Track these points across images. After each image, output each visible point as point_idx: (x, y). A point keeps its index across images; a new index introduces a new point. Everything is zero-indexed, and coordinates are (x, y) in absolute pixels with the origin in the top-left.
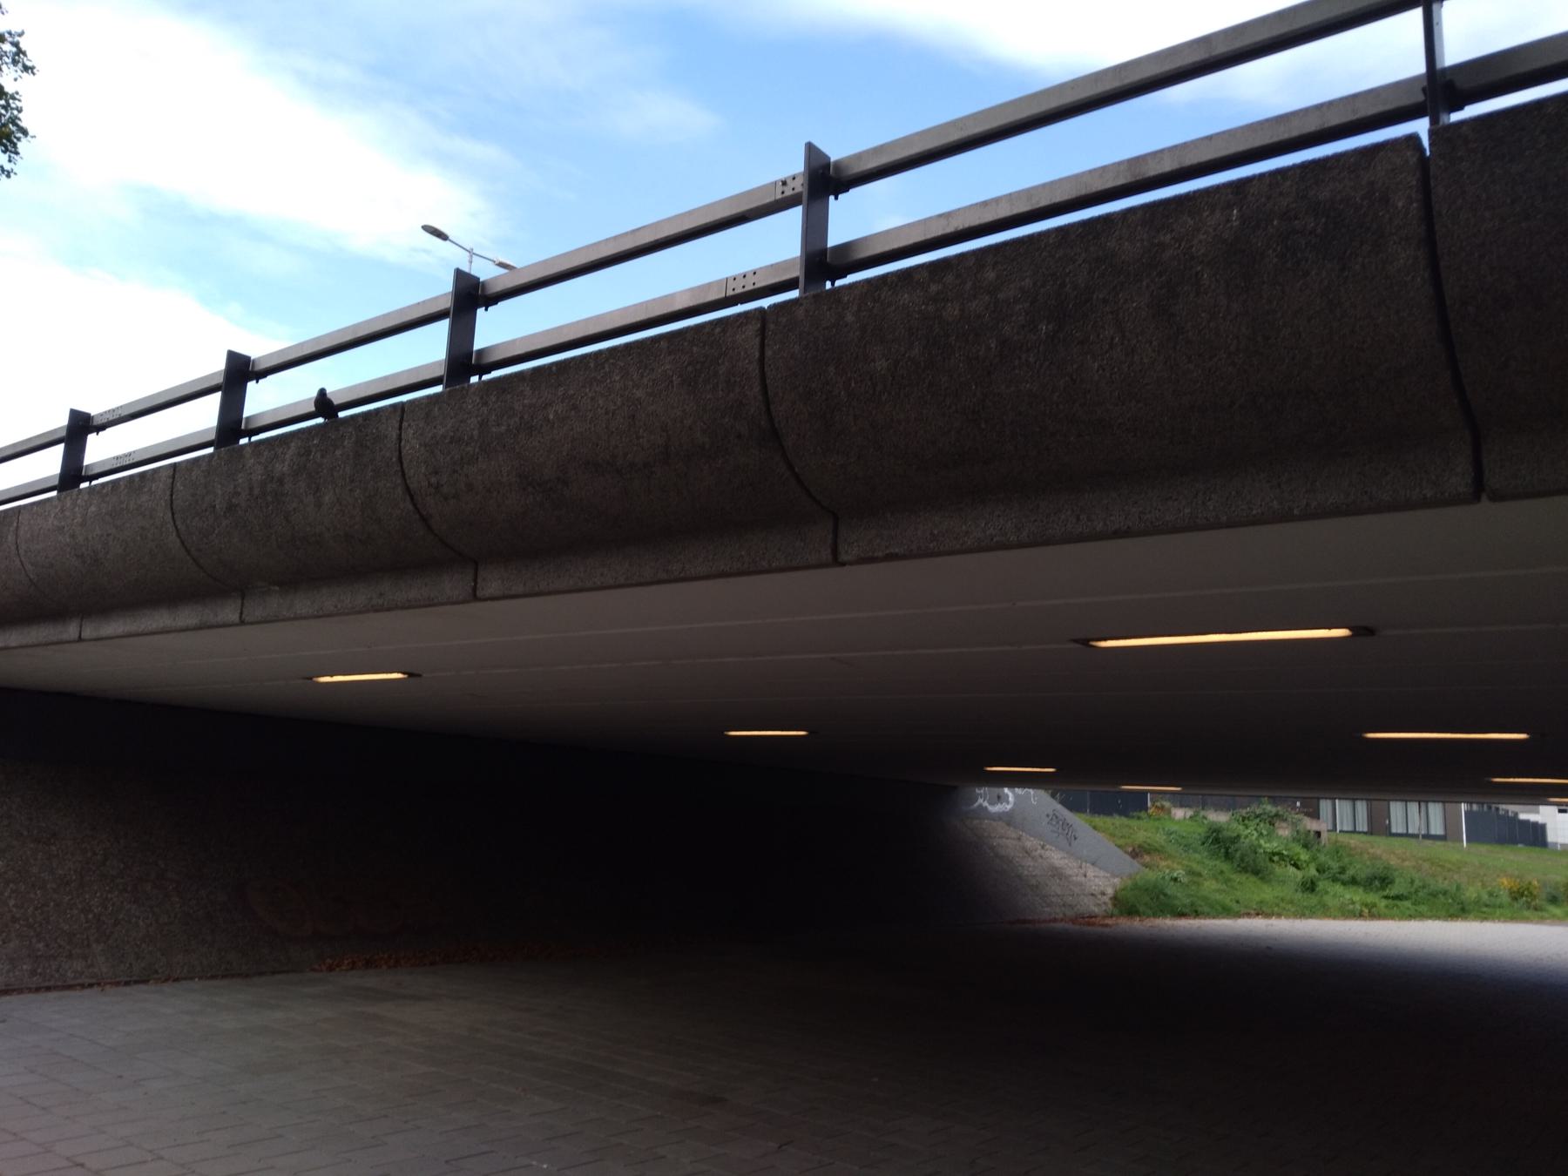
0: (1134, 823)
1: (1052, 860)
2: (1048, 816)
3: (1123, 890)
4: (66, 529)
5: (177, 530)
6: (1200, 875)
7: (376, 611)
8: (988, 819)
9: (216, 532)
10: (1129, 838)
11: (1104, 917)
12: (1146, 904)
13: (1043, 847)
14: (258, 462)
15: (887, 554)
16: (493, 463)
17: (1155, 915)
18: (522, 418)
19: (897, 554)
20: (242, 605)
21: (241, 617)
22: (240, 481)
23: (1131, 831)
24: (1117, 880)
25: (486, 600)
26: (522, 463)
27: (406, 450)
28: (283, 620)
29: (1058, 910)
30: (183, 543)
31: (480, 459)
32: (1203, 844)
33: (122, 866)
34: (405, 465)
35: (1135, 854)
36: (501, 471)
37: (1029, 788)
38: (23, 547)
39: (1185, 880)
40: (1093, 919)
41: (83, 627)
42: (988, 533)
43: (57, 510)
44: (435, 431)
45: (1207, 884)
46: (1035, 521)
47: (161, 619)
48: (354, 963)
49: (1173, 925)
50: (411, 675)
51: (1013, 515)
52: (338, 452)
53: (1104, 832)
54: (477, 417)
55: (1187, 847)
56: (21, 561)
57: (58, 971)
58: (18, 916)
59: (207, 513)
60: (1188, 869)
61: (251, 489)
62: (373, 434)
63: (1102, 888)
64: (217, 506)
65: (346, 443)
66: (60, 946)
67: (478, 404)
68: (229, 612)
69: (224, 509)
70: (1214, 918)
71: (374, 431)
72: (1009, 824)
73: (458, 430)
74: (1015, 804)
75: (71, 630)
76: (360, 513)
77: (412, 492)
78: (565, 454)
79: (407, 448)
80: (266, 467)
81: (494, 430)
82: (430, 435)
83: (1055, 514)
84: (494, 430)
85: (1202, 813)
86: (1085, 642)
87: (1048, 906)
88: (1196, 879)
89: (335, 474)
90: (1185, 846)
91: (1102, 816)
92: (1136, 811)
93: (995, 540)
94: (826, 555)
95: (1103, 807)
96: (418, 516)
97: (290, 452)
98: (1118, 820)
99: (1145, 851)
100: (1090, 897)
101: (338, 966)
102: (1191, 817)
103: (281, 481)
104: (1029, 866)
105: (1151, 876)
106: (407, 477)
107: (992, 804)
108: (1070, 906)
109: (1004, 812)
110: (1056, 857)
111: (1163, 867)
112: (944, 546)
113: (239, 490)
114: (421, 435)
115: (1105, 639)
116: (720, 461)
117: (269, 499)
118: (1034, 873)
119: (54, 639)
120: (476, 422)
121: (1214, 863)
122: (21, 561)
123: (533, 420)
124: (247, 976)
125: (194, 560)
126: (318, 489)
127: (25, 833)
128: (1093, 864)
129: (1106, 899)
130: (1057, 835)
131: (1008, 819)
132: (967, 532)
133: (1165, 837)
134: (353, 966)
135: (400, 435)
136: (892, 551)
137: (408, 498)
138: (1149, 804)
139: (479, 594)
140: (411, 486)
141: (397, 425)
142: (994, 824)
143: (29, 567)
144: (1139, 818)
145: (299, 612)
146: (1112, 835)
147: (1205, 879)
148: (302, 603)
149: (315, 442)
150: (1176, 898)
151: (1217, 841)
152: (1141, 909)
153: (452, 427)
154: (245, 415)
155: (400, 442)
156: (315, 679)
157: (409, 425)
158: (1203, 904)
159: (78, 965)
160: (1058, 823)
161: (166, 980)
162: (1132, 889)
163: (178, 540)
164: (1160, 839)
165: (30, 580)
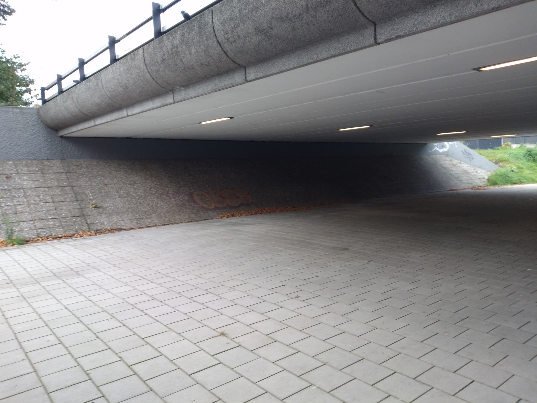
0: (496, 151)
1: (464, 168)
2: (462, 151)
3: (491, 176)
4: (115, 78)
5: (148, 71)
6: (522, 168)
7: (215, 91)
8: (439, 155)
9: (160, 70)
10: (494, 157)
11: (484, 186)
12: (500, 180)
13: (460, 163)
14: (169, 42)
15: (396, 36)
16: (245, 25)
17: (504, 184)
18: (253, 5)
19: (400, 35)
20: (173, 96)
21: (174, 100)
22: (164, 49)
23: (495, 154)
24: (489, 173)
25: (250, 81)
26: (255, 23)
27: (216, 27)
28: (187, 99)
29: (466, 185)
30: (151, 76)
31: (241, 25)
32: (524, 156)
33: (156, 190)
34: (216, 33)
35: (496, 163)
36: (248, 28)
37: (455, 141)
38: (104, 86)
39: (516, 171)
40: (480, 187)
41: (128, 111)
42: (438, 19)
43: (111, 71)
44: (224, 17)
45: (525, 171)
46: (457, 10)
47: (149, 105)
48: (228, 216)
49: (511, 187)
50: (231, 118)
51: (448, 10)
52: (193, 32)
53: (484, 155)
54: (237, 8)
55: (518, 158)
56: (105, 91)
57: (144, 222)
58: (130, 207)
59: (157, 64)
60: (518, 166)
61: (168, 52)
62: (204, 22)
63: (483, 176)
64: (159, 60)
65: (195, 28)
66: (143, 215)
67: (237, 3)
68: (169, 99)
69: (161, 61)
70: (528, 183)
71: (204, 21)
72: (447, 156)
73: (232, 15)
74: (449, 148)
75: (124, 113)
76: (204, 54)
77: (220, 43)
78: (270, 16)
79: (216, 26)
80: (171, 43)
81: (244, 12)
82: (223, 19)
83: (467, 5)
84: (244, 12)
85: (524, 145)
86: (478, 69)
87: (463, 184)
88: (521, 170)
89: (194, 41)
90: (517, 158)
91: (483, 150)
92: (496, 146)
93: (440, 22)
94: (372, 41)
95: (484, 146)
96: (223, 52)
97: (178, 36)
98: (490, 151)
99: (500, 161)
100: (479, 180)
101: (224, 217)
102: (519, 147)
103: (177, 47)
104: (455, 170)
105: (503, 170)
106: (217, 37)
107: (440, 149)
108: (471, 183)
109: (445, 152)
110: (465, 166)
111: (508, 166)
112: (420, 28)
113: (165, 53)
114: (220, 19)
115: (486, 67)
116: (328, 8)
117: (174, 54)
118: (457, 173)
119: (120, 117)
120: (237, 10)
121: (529, 163)
122: (105, 91)
123: (257, 5)
124: (198, 221)
125: (156, 82)
126: (189, 48)
127: (126, 182)
128: (480, 168)
129: (485, 180)
130: (465, 158)
131: (446, 154)
132: (429, 21)
133: (508, 155)
134: (228, 217)
135: (213, 21)
136: (398, 34)
137: (219, 45)
138: (502, 144)
139: (248, 79)
140: (220, 40)
141: (211, 17)
142: (441, 156)
143: (108, 93)
144: (498, 149)
145: (191, 96)
146: (487, 156)
147: (525, 170)
148: (192, 92)
149: (185, 30)
150: (513, 178)
151: (530, 155)
152: (499, 182)
153: (229, 14)
154: (162, 27)
155: (213, 24)
156: (201, 123)
157: (215, 16)
158: (523, 179)
159: (149, 221)
160: (466, 153)
161: (175, 224)
162: (495, 176)
163: (149, 75)
164: (506, 156)
165: (109, 97)
